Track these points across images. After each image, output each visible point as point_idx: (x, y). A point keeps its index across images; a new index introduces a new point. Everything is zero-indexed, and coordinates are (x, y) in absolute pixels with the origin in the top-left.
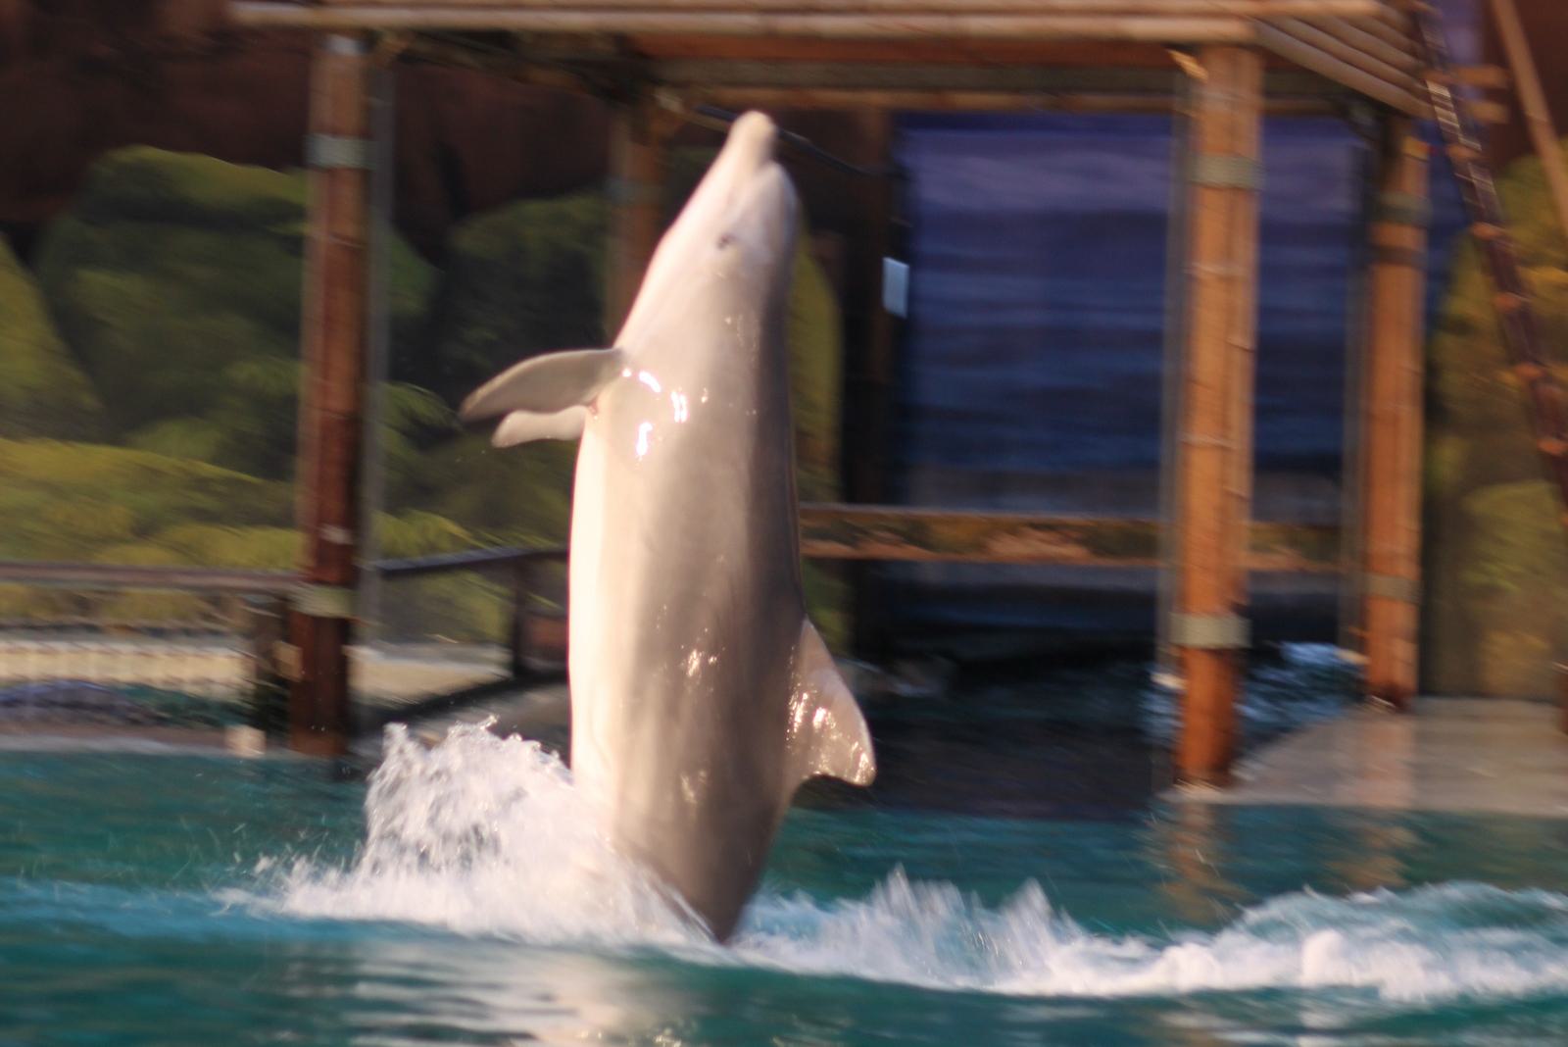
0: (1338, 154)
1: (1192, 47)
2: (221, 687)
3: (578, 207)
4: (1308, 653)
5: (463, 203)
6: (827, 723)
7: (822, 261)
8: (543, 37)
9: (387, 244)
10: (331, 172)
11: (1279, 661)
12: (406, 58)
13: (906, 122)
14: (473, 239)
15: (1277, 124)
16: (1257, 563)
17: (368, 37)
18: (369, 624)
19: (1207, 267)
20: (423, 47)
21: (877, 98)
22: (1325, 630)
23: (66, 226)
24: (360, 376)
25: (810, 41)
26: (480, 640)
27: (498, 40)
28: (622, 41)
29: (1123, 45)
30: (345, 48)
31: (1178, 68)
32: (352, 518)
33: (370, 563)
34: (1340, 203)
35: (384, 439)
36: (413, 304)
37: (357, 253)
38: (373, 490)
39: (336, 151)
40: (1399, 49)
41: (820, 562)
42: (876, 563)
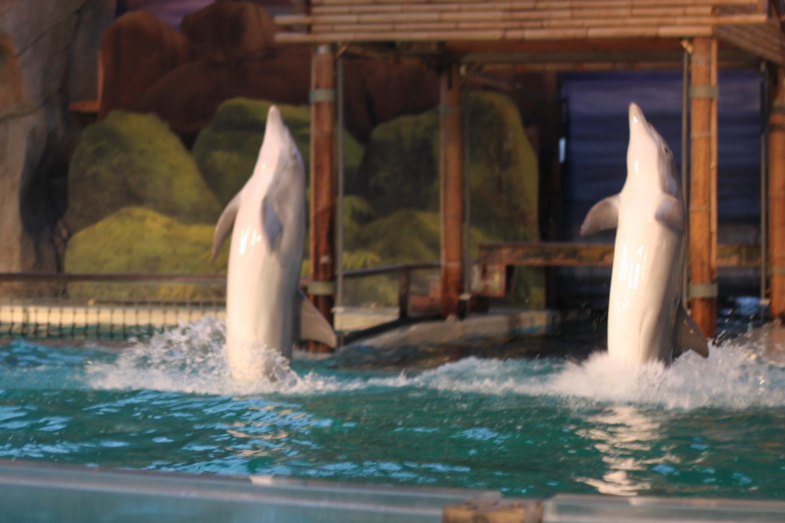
0: (754, 86)
1: (691, 39)
2: (249, 451)
3: (425, 118)
4: (746, 302)
5: (375, 121)
6: (484, 402)
7: (530, 139)
8: (409, 44)
9: (341, 133)
10: (318, 105)
11: (734, 305)
12: (347, 55)
13: (564, 78)
14: (379, 133)
15: (724, 75)
16: (725, 263)
17: (333, 46)
18: (339, 298)
19: (697, 133)
20: (357, 51)
21: (552, 67)
22: (753, 290)
23: (205, 133)
24: (333, 193)
25: (522, 42)
26: (388, 305)
27: (390, 45)
28: (441, 44)
29: (656, 40)
30: (323, 50)
31: (683, 50)
32: (332, 251)
33: (340, 272)
34: (756, 106)
35: (343, 220)
36: (356, 161)
37: (332, 137)
38: (339, 243)
39: (321, 95)
40: (530, 355)
41: (530, 267)
42: (558, 268)
